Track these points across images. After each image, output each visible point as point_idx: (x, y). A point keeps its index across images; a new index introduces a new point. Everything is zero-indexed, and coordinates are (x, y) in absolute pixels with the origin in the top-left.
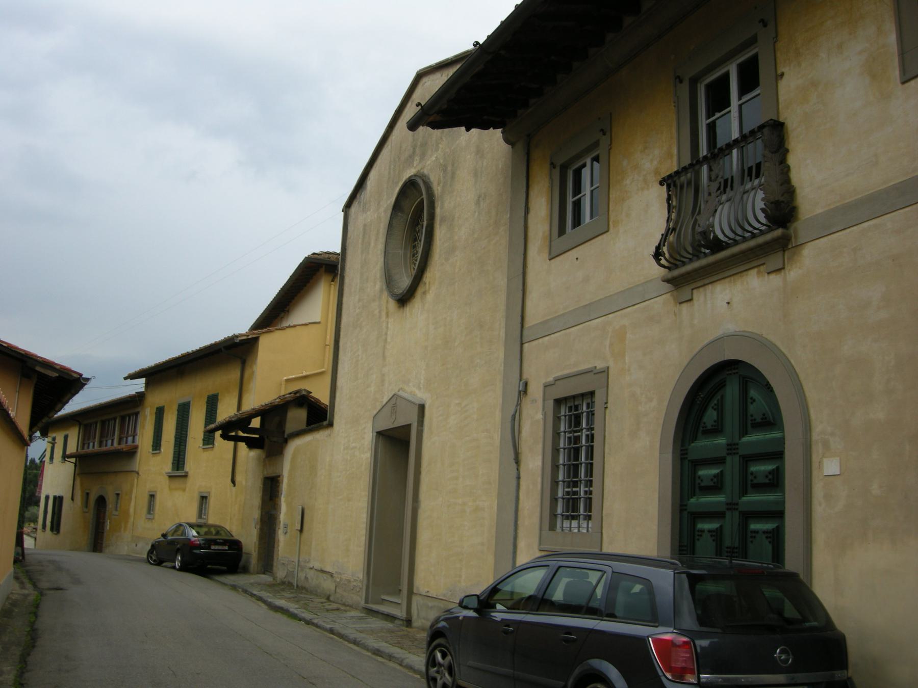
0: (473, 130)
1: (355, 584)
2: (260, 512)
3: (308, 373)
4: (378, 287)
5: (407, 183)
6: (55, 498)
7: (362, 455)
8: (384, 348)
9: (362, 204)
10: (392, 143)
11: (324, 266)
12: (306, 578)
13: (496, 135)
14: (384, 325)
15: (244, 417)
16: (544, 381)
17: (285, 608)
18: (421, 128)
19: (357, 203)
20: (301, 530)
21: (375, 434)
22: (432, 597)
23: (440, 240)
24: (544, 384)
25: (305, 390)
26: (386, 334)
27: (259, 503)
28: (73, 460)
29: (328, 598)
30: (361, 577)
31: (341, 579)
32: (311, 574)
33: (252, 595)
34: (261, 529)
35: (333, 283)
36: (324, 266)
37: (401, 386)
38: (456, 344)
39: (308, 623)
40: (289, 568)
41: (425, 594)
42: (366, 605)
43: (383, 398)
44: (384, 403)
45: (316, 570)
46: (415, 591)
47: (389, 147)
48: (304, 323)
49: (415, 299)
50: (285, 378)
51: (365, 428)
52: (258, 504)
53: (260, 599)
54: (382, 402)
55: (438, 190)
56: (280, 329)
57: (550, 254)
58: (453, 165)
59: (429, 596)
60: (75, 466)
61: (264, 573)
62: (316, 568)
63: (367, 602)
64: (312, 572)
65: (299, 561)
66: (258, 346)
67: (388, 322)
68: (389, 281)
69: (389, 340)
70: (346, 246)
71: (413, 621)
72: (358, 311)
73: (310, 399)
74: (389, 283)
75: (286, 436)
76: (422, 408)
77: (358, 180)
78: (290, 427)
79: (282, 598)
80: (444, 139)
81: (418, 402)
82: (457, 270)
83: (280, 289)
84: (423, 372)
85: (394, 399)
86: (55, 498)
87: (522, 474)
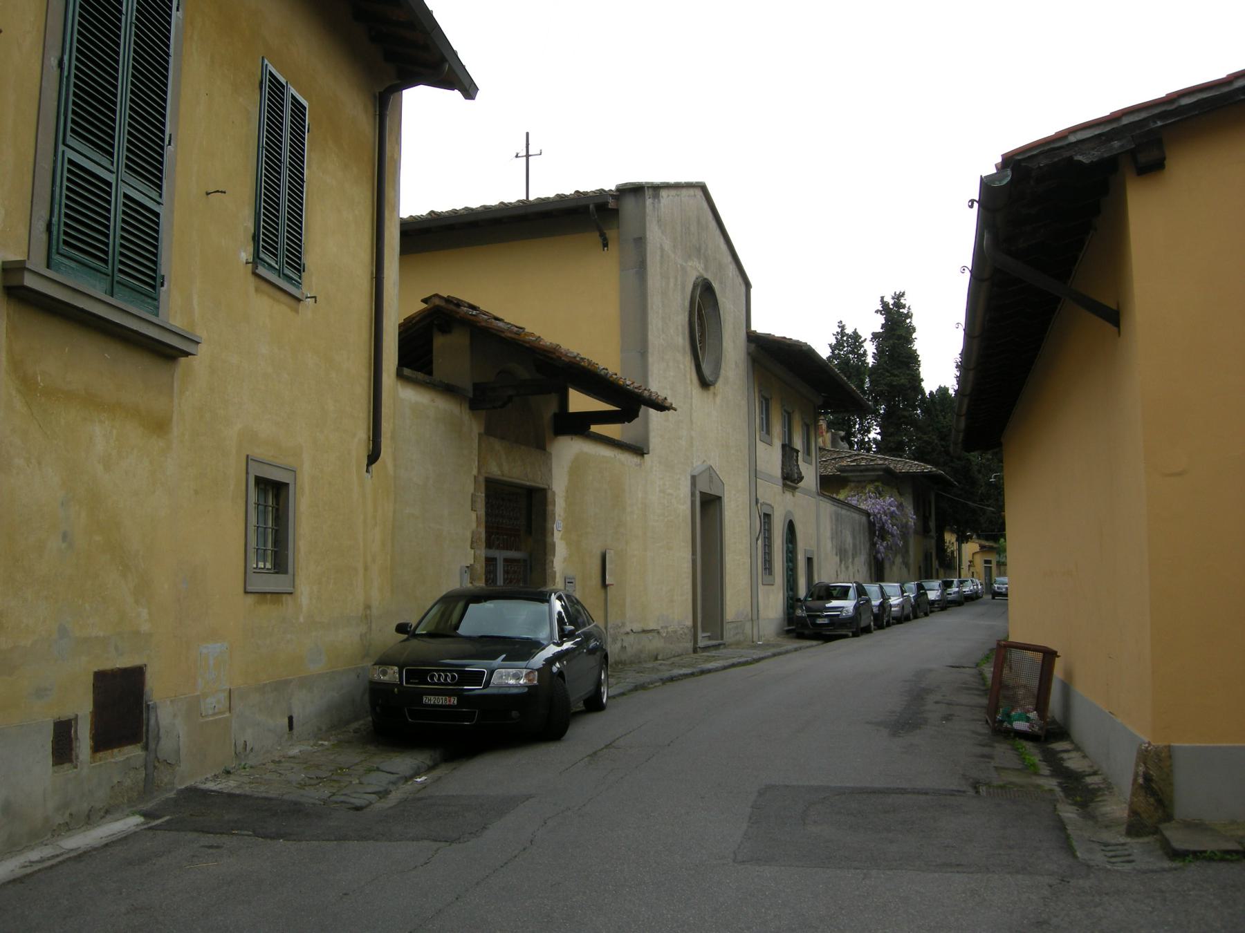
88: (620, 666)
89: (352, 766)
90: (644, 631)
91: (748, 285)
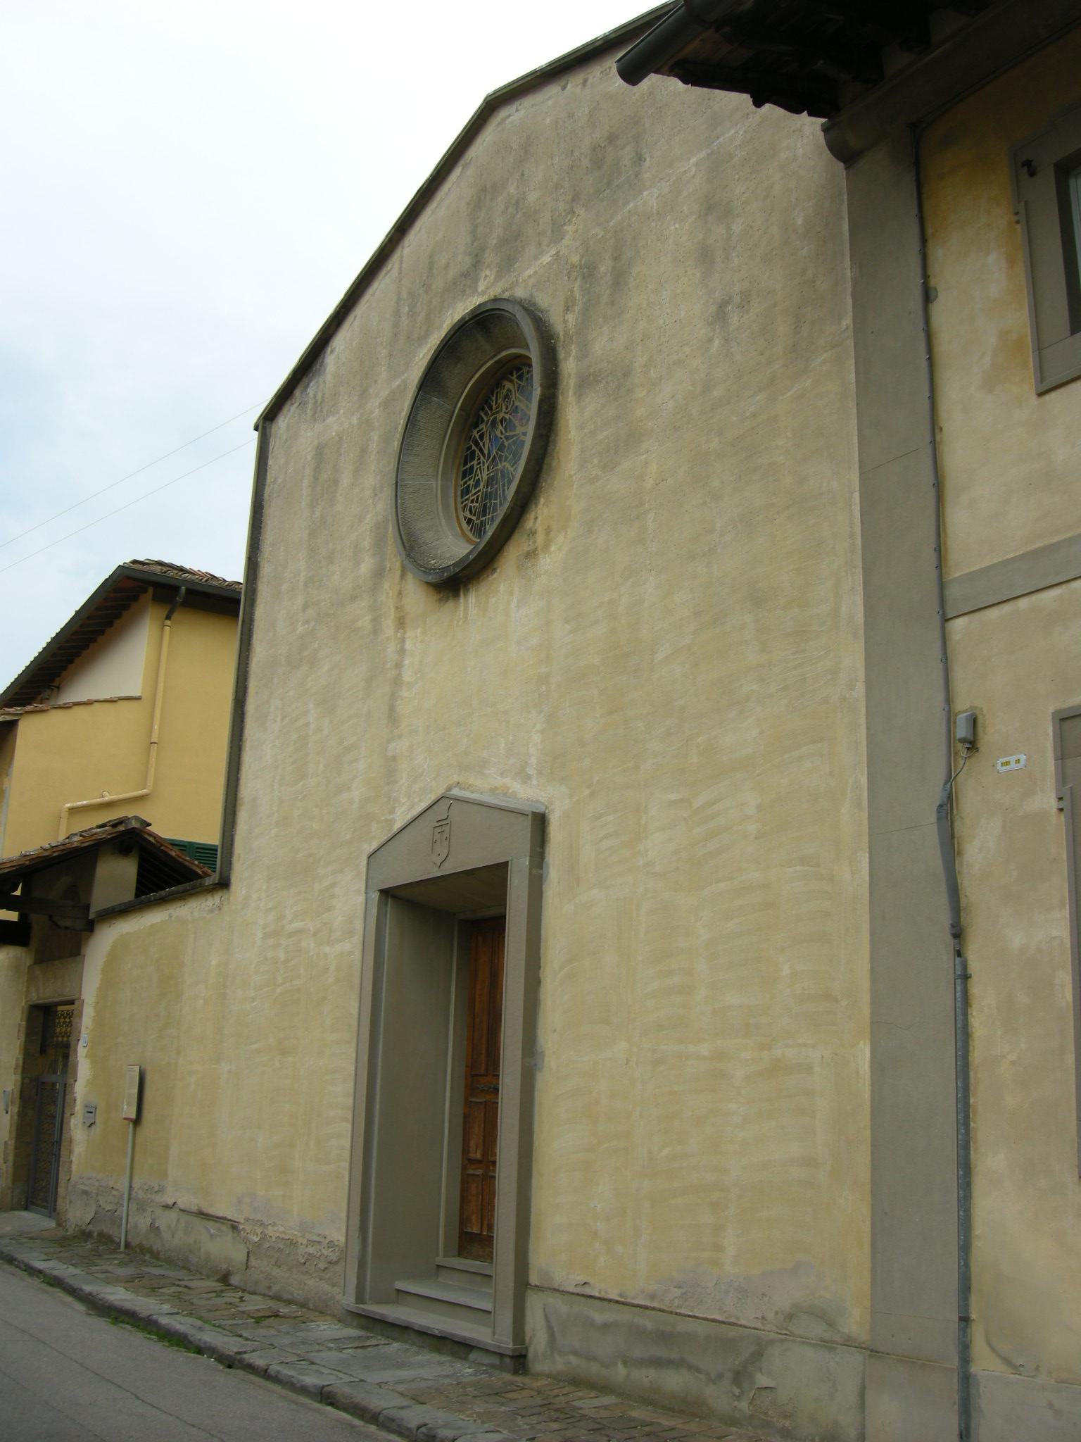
0: (768, 107)
1: (311, 1250)
2: (19, 1078)
3: (115, 797)
4: (367, 566)
5: (466, 323)
7: (327, 949)
8: (393, 697)
9: (310, 406)
10: (401, 262)
11: (151, 590)
12: (154, 1229)
13: (809, 127)
14: (392, 647)
15: (6, 871)
16: (1051, 709)
17: (144, 1313)
18: (652, 75)
19: (293, 408)
20: (137, 1121)
21: (375, 896)
22: (600, 1299)
23: (581, 428)
24: (1054, 714)
25: (137, 818)
26: (398, 665)
27: (17, 1059)
29: (225, 1279)
30: (339, 1236)
31: (264, 1238)
32: (166, 1220)
33: (33, 1272)
34: (22, 1114)
35: (168, 622)
36: (151, 590)
37: (455, 778)
38: (659, 656)
39: (231, 1362)
40: (101, 1203)
41: (572, 1289)
42: (361, 1306)
43: (392, 811)
44: (398, 825)
45: (181, 1210)
46: (534, 1279)
47: (395, 272)
48: (108, 697)
49: (495, 575)
50: (68, 805)
51: (333, 885)
52: (14, 1062)
53: (56, 1282)
54: (392, 822)
55: (565, 321)
56: (60, 708)
57: (1041, 375)
58: (616, 258)
59: (591, 1297)
61: (26, 1209)
62: (182, 1206)
63: (360, 1299)
64: (173, 1215)
65: (131, 1187)
66: (15, 742)
67: (403, 641)
68: (411, 547)
69: (407, 676)
70: (262, 500)
71: (530, 1355)
72: (301, 629)
73: (146, 836)
74: (412, 548)
75: (92, 916)
76: (540, 822)
77: (302, 356)
78: (100, 897)
79: (110, 1280)
80: (580, 211)
81: (528, 809)
82: (649, 483)
83: (32, 659)
84: (537, 738)
85: (444, 805)
87: (974, 966)
88: (147, 1257)
89: (502, 1393)
90: (202, 1214)
91: (493, 105)
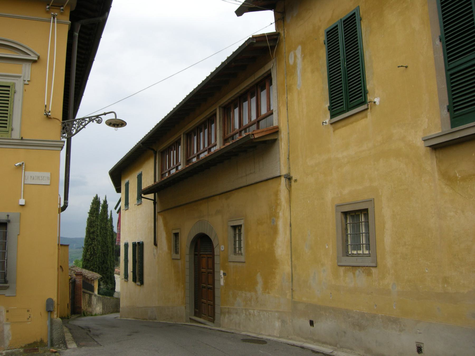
6: (134, 245)
28: (151, 196)
60: (155, 203)
86: (134, 245)
